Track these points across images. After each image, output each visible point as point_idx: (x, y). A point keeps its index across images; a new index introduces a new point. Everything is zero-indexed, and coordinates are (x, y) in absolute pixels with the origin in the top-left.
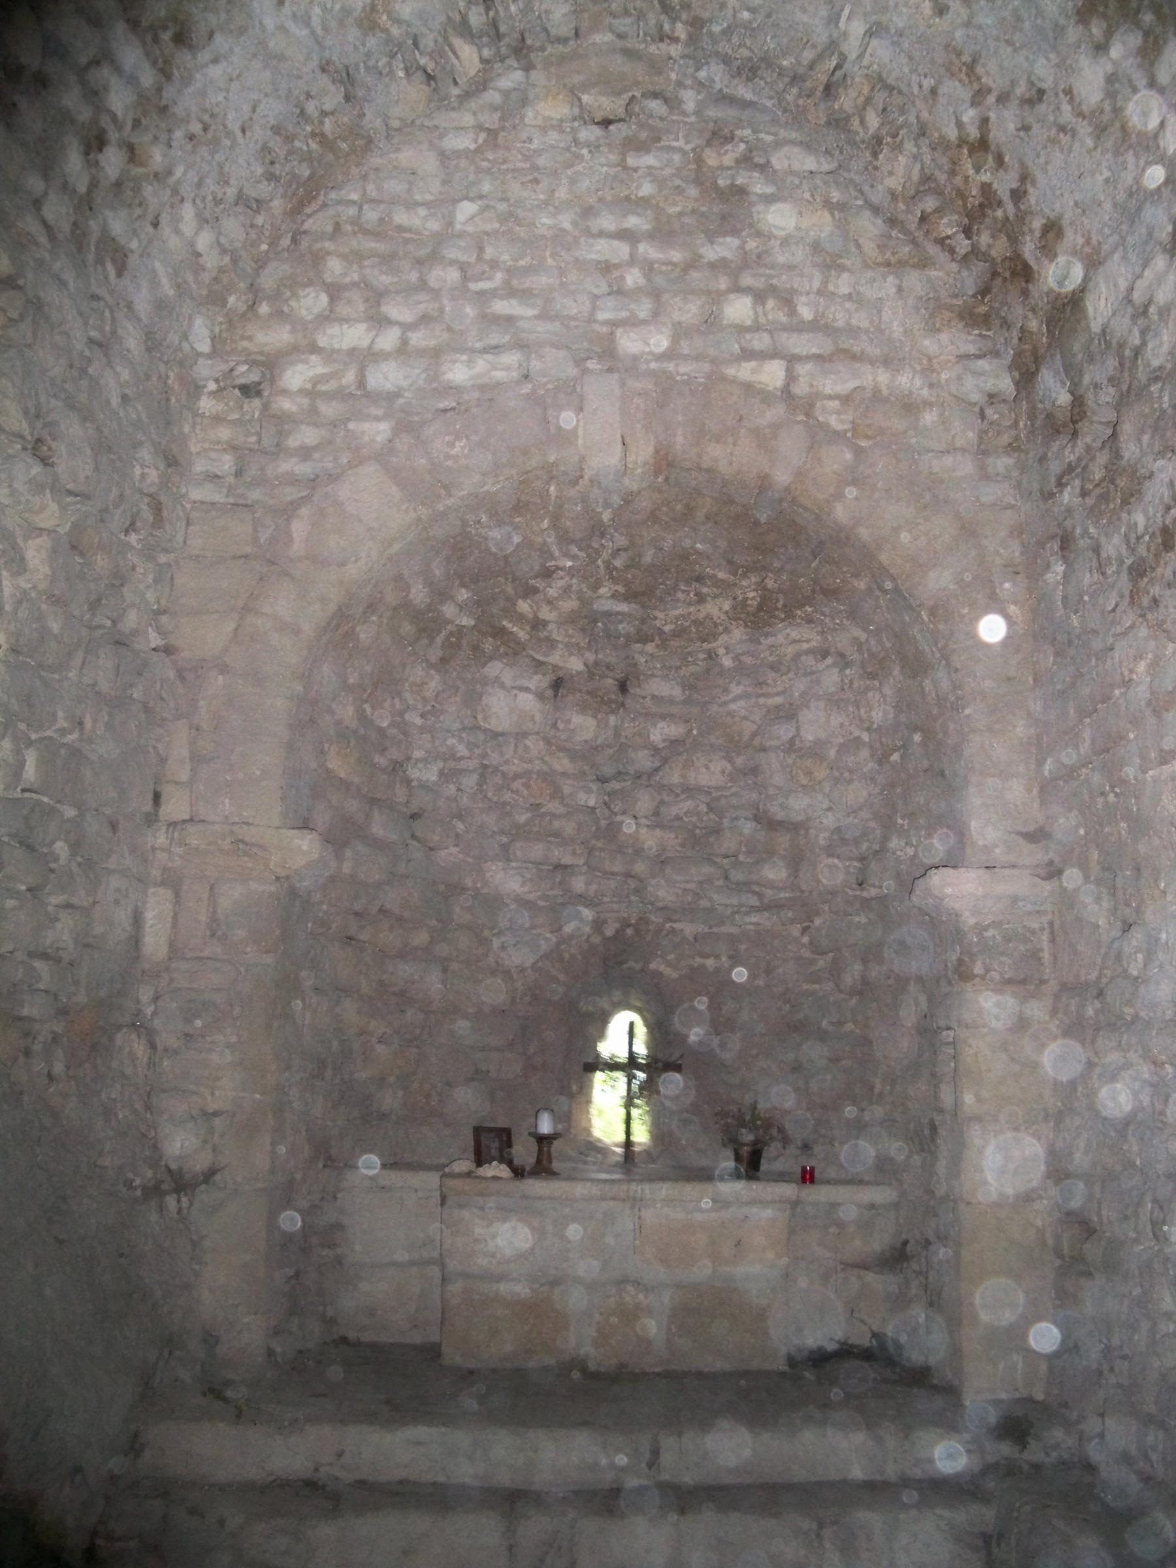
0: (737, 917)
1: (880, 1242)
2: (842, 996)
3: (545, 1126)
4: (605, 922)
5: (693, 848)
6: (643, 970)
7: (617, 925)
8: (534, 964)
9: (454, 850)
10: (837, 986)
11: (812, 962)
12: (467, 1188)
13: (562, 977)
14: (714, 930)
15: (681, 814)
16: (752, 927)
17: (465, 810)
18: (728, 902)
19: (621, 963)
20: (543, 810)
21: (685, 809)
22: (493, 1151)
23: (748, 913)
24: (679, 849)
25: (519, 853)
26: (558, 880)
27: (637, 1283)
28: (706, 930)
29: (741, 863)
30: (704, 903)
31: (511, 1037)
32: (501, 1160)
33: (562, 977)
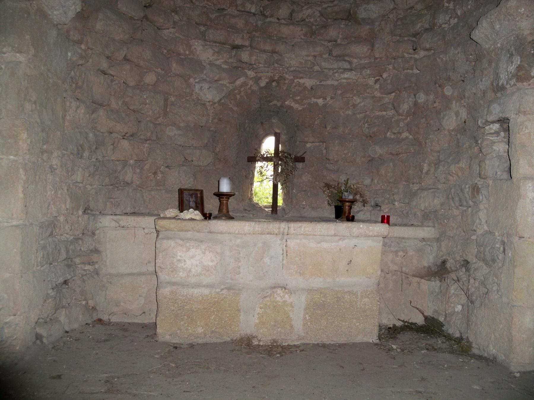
0: (336, 75)
1: (429, 260)
2: (401, 117)
3: (225, 187)
4: (260, 78)
5: (311, 37)
6: (281, 106)
7: (267, 80)
8: (221, 100)
9: (172, 30)
10: (397, 112)
11: (381, 99)
12: (172, 226)
13: (235, 109)
14: (323, 83)
15: (305, 16)
16: (345, 81)
17: (179, 7)
18: (331, 67)
19: (270, 102)
20: (225, 12)
21: (307, 14)
22: (191, 203)
23: (342, 73)
24: (303, 37)
25: (211, 36)
26: (233, 54)
27: (284, 288)
28: (318, 83)
29: (340, 45)
30: (316, 68)
31: (206, 141)
32: (196, 209)
33: (235, 109)
